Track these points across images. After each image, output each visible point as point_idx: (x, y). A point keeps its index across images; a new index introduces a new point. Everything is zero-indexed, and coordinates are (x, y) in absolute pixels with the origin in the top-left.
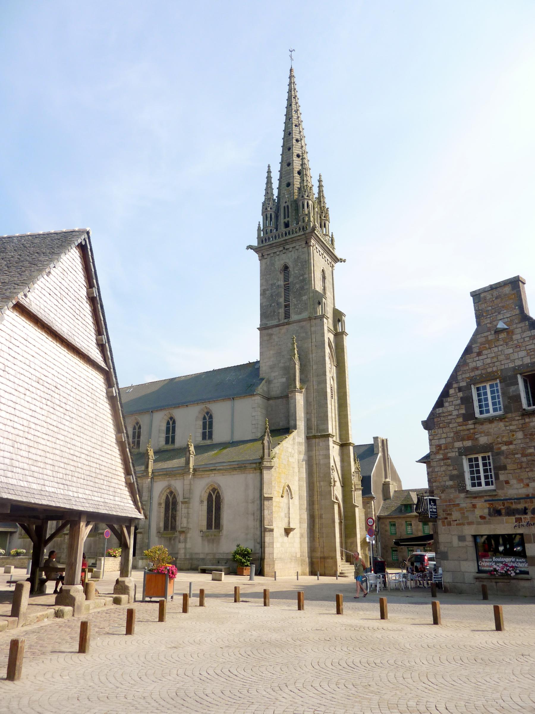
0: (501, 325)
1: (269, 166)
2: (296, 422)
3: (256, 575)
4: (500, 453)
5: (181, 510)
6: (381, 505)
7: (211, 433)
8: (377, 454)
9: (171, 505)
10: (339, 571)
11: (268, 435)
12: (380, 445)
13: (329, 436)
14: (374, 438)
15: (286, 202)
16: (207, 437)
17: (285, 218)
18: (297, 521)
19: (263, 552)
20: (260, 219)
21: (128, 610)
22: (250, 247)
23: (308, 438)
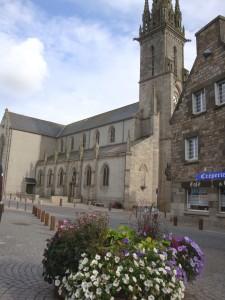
0: (208, 51)
4: (202, 136)
9: (89, 172)
18: (151, 182)
20: (141, 23)
22: (135, 39)
23: (161, 140)
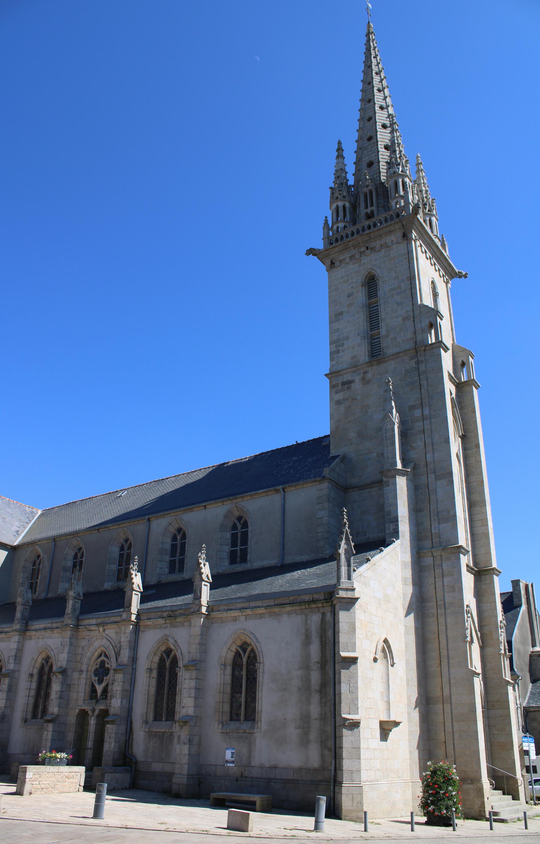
1: (339, 143)
3: (327, 816)
5: (186, 681)
6: (529, 690)
8: (520, 606)
10: (488, 809)
11: (347, 539)
12: (523, 592)
13: (460, 552)
14: (513, 582)
15: (368, 186)
16: (238, 559)
17: (366, 207)
19: (338, 768)
22: (311, 252)
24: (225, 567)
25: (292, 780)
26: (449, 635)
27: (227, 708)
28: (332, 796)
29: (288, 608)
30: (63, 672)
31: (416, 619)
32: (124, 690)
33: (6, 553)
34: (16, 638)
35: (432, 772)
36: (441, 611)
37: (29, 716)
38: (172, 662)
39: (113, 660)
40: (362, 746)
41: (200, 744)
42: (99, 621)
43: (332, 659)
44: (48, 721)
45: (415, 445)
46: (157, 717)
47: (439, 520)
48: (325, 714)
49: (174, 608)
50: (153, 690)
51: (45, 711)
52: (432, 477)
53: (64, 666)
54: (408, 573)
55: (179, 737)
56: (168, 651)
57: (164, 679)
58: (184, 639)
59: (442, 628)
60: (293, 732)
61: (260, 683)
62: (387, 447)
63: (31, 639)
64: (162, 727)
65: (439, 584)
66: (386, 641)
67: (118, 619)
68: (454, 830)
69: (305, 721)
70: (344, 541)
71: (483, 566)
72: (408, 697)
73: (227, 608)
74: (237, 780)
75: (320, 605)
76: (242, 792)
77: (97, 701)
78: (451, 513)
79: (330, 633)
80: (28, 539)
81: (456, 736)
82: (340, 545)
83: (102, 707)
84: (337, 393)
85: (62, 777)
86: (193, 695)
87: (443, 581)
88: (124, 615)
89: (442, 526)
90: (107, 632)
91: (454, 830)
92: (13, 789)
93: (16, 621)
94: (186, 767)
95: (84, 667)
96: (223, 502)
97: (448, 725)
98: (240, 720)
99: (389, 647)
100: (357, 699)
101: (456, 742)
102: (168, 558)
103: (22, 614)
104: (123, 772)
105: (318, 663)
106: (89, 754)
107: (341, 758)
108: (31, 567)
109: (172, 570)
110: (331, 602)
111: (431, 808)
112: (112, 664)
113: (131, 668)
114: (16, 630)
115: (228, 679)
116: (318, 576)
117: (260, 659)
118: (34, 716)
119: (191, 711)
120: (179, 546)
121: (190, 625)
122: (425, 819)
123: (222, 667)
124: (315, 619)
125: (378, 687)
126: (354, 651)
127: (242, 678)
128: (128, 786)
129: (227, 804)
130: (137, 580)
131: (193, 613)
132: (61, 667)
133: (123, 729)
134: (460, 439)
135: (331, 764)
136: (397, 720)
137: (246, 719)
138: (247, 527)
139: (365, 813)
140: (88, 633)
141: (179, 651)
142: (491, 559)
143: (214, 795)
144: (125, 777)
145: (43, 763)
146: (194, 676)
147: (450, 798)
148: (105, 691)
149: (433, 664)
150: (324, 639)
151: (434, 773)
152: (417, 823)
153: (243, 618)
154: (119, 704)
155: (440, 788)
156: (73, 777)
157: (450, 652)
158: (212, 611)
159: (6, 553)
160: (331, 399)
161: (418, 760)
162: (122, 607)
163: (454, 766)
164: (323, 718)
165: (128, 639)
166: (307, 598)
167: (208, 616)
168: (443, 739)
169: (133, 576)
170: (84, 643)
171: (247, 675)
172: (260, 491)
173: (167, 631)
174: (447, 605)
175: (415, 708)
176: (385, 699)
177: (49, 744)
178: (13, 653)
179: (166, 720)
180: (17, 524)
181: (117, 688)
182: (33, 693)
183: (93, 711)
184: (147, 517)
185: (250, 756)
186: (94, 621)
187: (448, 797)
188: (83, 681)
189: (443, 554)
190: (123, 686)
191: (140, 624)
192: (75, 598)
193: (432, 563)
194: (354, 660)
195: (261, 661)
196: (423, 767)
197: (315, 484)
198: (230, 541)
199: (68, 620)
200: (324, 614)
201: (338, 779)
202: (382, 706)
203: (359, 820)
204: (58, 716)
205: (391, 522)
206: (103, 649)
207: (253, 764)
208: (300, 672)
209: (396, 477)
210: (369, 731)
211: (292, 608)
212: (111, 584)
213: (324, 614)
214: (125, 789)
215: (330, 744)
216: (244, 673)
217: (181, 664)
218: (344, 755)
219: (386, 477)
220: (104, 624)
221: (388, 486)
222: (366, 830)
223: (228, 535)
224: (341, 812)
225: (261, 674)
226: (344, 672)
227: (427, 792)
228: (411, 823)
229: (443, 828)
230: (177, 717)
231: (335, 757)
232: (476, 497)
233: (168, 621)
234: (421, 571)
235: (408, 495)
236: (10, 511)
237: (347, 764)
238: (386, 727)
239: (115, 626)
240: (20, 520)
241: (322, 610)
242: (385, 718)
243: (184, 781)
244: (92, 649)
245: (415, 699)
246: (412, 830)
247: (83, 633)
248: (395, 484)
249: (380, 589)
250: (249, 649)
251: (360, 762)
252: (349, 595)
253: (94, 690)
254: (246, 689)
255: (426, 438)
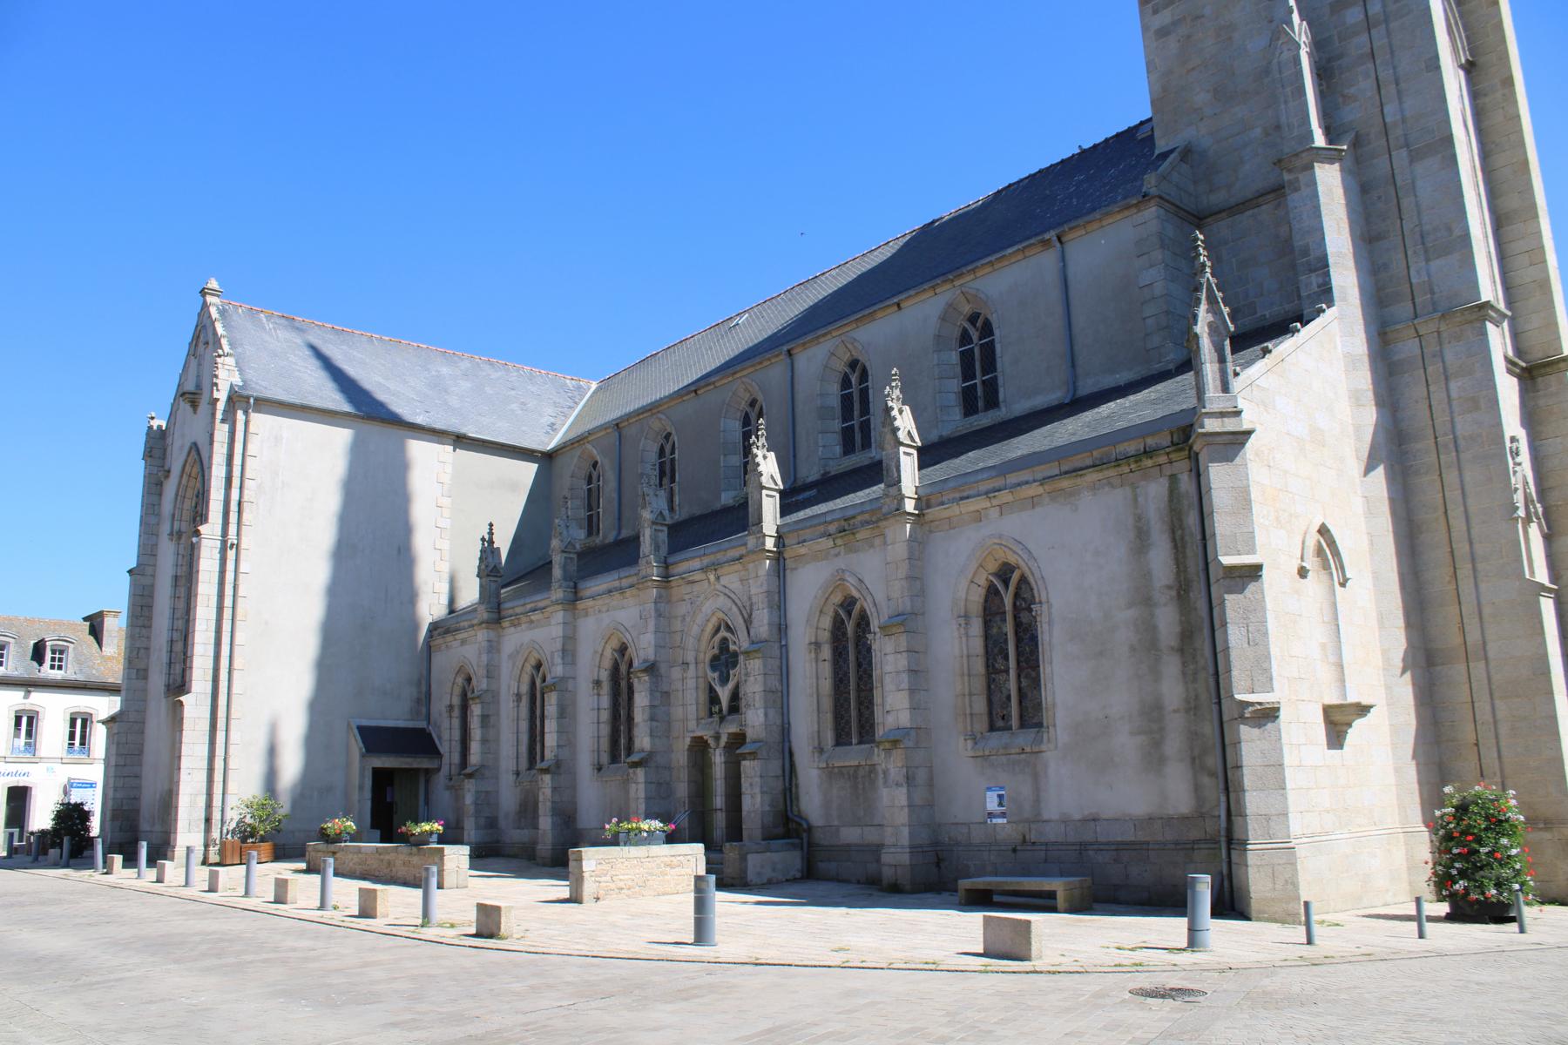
2: (1328, 274)
3: (1217, 912)
5: (889, 658)
7: (992, 388)
11: (1212, 300)
13: (1484, 319)
16: (981, 404)
19: (1233, 811)
21: (1341, 747)
24: (955, 422)
25: (1133, 843)
26: (1472, 509)
27: (980, 705)
28: (1225, 871)
29: (1092, 476)
30: (651, 668)
31: (1391, 479)
32: (767, 691)
33: (535, 466)
34: (559, 616)
35: (1457, 808)
36: (1448, 458)
37: (605, 759)
38: (858, 625)
39: (742, 633)
40: (1287, 761)
41: (931, 784)
42: (706, 561)
43: (1202, 576)
44: (635, 765)
45: (1352, 90)
46: (841, 739)
47: (1426, 251)
48: (1197, 697)
49: (849, 513)
50: (827, 685)
51: (630, 750)
52: (1400, 157)
53: (652, 658)
54: (1364, 379)
55: (885, 772)
56: (849, 604)
57: (846, 661)
58: (876, 573)
59: (1454, 495)
60: (1127, 743)
61: (1047, 647)
62: (1286, 102)
63: (586, 615)
64: (853, 756)
65: (1438, 395)
66: (1323, 531)
67: (743, 550)
68: (1522, 931)
69: (1152, 715)
70: (1203, 307)
71: (1540, 355)
72: (1385, 652)
73: (957, 495)
74: (1014, 850)
75: (1163, 459)
76: (1027, 873)
77: (722, 719)
78: (1457, 232)
79: (1192, 519)
80: (572, 435)
81: (1504, 730)
82: (1195, 317)
83: (733, 729)
84: (1155, 12)
85: (658, 866)
86: (905, 685)
87: (1448, 390)
88: (751, 541)
89: (1435, 265)
90: (724, 581)
91: (1522, 931)
92: (565, 892)
93: (555, 585)
94: (906, 831)
95: (690, 657)
96: (933, 288)
97: (1483, 707)
98: (1010, 728)
99: (1332, 543)
100: (1268, 657)
101: (1502, 743)
102: (837, 425)
103: (564, 568)
104: (781, 848)
105: (1169, 587)
106: (720, 820)
107: (1241, 789)
108: (585, 487)
109: (848, 447)
110: (1190, 449)
111: (1460, 886)
112: (741, 642)
113: (777, 646)
114: (557, 603)
115: (978, 645)
116: (1153, 402)
117: (1040, 593)
118: (614, 758)
119: (904, 719)
120: (856, 398)
121: (885, 543)
122: (1444, 908)
123: (962, 621)
124: (1155, 492)
125: (1314, 634)
126: (1252, 551)
127: (1006, 641)
128: (798, 875)
129: (996, 898)
130: (768, 466)
131: (885, 517)
132: (645, 661)
133: (775, 766)
134: (1462, 73)
135: (1218, 805)
136: (1365, 702)
137: (1023, 724)
138: (991, 333)
139: (1307, 904)
140: (688, 588)
141: (869, 599)
142: (1559, 338)
143: (965, 884)
144: (788, 859)
145: (614, 842)
146: (903, 646)
147: (1506, 861)
148: (735, 696)
149: (1438, 577)
150: (1179, 533)
151: (1462, 809)
152: (1431, 919)
153: (994, 513)
154: (762, 719)
155: (1479, 841)
156: (680, 865)
157: (1477, 546)
158: (928, 507)
159: (535, 466)
160: (1145, 28)
161: (1416, 786)
162: (744, 528)
163: (1512, 792)
164: (1192, 707)
165: (765, 588)
166: (1131, 447)
167: (919, 517)
168: (1471, 738)
169: (759, 459)
170: (682, 609)
171: (1016, 633)
172: (1010, 251)
173: (840, 563)
174: (1461, 443)
175: (1403, 672)
176: (1332, 659)
177: (642, 807)
178: (559, 645)
179: (860, 743)
180: (550, 411)
181: (754, 689)
182: (605, 715)
183: (717, 738)
184: (785, 348)
185: (1037, 801)
186: (696, 564)
187: (1500, 861)
188: (691, 683)
189: (1443, 327)
190: (765, 684)
191: (786, 555)
192: (654, 523)
193: (1418, 352)
194: (1254, 572)
195: (1044, 599)
196: (1431, 797)
197: (1126, 213)
198: (958, 369)
199: (651, 567)
200: (1173, 478)
201: (1237, 835)
202: (1325, 674)
203: (1290, 919)
204: (651, 754)
205: (1311, 271)
206: (721, 615)
207: (1045, 817)
208: (1131, 613)
209: (1313, 167)
210: (1300, 729)
211: (1101, 475)
212: (732, 493)
213: (1173, 478)
214: (795, 880)
215: (1213, 761)
216: (1009, 628)
217: (874, 625)
218: (1248, 782)
219: (1290, 171)
220: (715, 566)
221: (1297, 190)
222: (1310, 942)
223: (954, 357)
224: (1248, 905)
225: (1045, 626)
226: (1231, 600)
227: (1449, 851)
228: (1418, 918)
229: (1492, 927)
230: (880, 732)
231: (1227, 789)
232: (1511, 202)
233: (839, 542)
234: (1391, 374)
235: (1348, 204)
236: (534, 389)
237: (1254, 801)
238: (1337, 717)
239: (738, 566)
240: (555, 404)
241: (1168, 470)
242: (1333, 699)
243: (905, 859)
244: (700, 619)
245: (1401, 655)
246: (1421, 936)
247: (679, 590)
248: (1314, 183)
249: (1300, 425)
250: (1015, 577)
251: (1285, 797)
252: (1230, 425)
253: (714, 699)
254: (1018, 662)
255: (1379, 70)
